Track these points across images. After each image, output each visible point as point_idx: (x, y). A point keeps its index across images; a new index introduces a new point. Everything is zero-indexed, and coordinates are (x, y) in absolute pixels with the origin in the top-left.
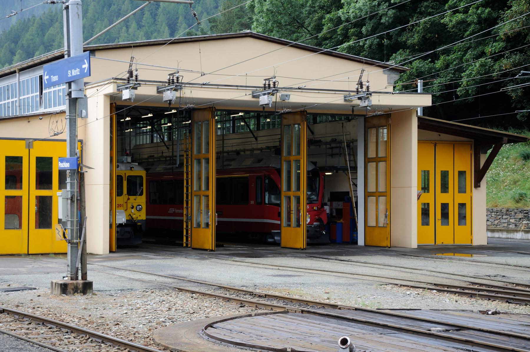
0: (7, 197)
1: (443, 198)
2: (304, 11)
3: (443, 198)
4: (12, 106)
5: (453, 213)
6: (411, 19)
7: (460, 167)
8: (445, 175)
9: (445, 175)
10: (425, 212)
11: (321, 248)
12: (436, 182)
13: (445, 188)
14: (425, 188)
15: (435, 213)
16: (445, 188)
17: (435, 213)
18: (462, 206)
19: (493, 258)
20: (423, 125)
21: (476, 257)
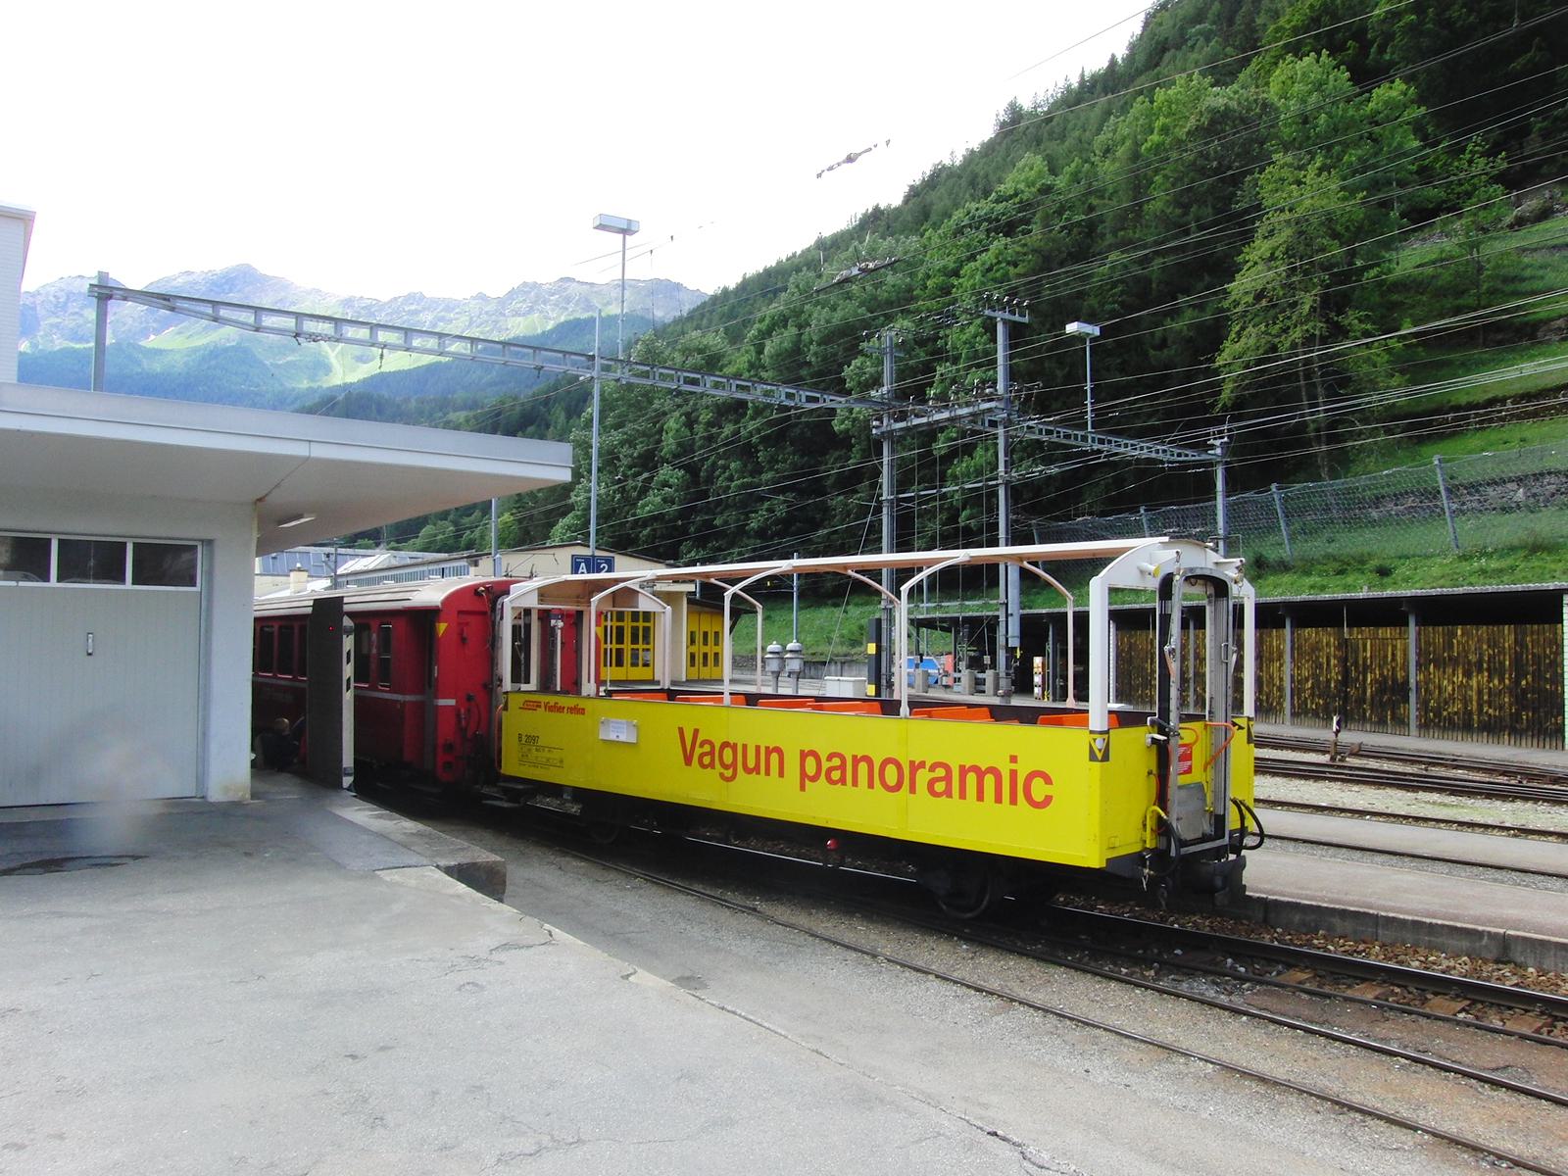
0: (1110, 611)
1: (706, 649)
2: (1092, 115)
3: (706, 649)
4: (547, 634)
5: (711, 658)
6: (1408, 376)
7: (704, 628)
8: (706, 634)
9: (706, 634)
10: (692, 657)
11: (1285, 1041)
12: (699, 638)
13: (705, 643)
14: (692, 641)
15: (699, 659)
16: (705, 643)
17: (699, 659)
18: (716, 654)
19: (504, 637)
20: (690, 602)
21: (1550, 838)
